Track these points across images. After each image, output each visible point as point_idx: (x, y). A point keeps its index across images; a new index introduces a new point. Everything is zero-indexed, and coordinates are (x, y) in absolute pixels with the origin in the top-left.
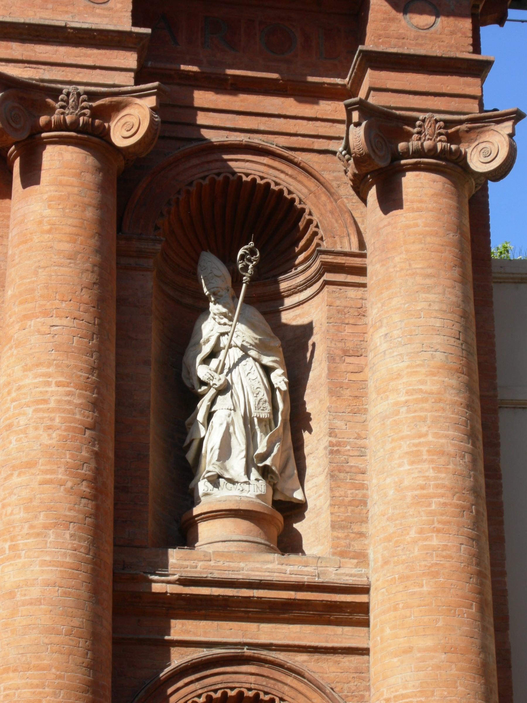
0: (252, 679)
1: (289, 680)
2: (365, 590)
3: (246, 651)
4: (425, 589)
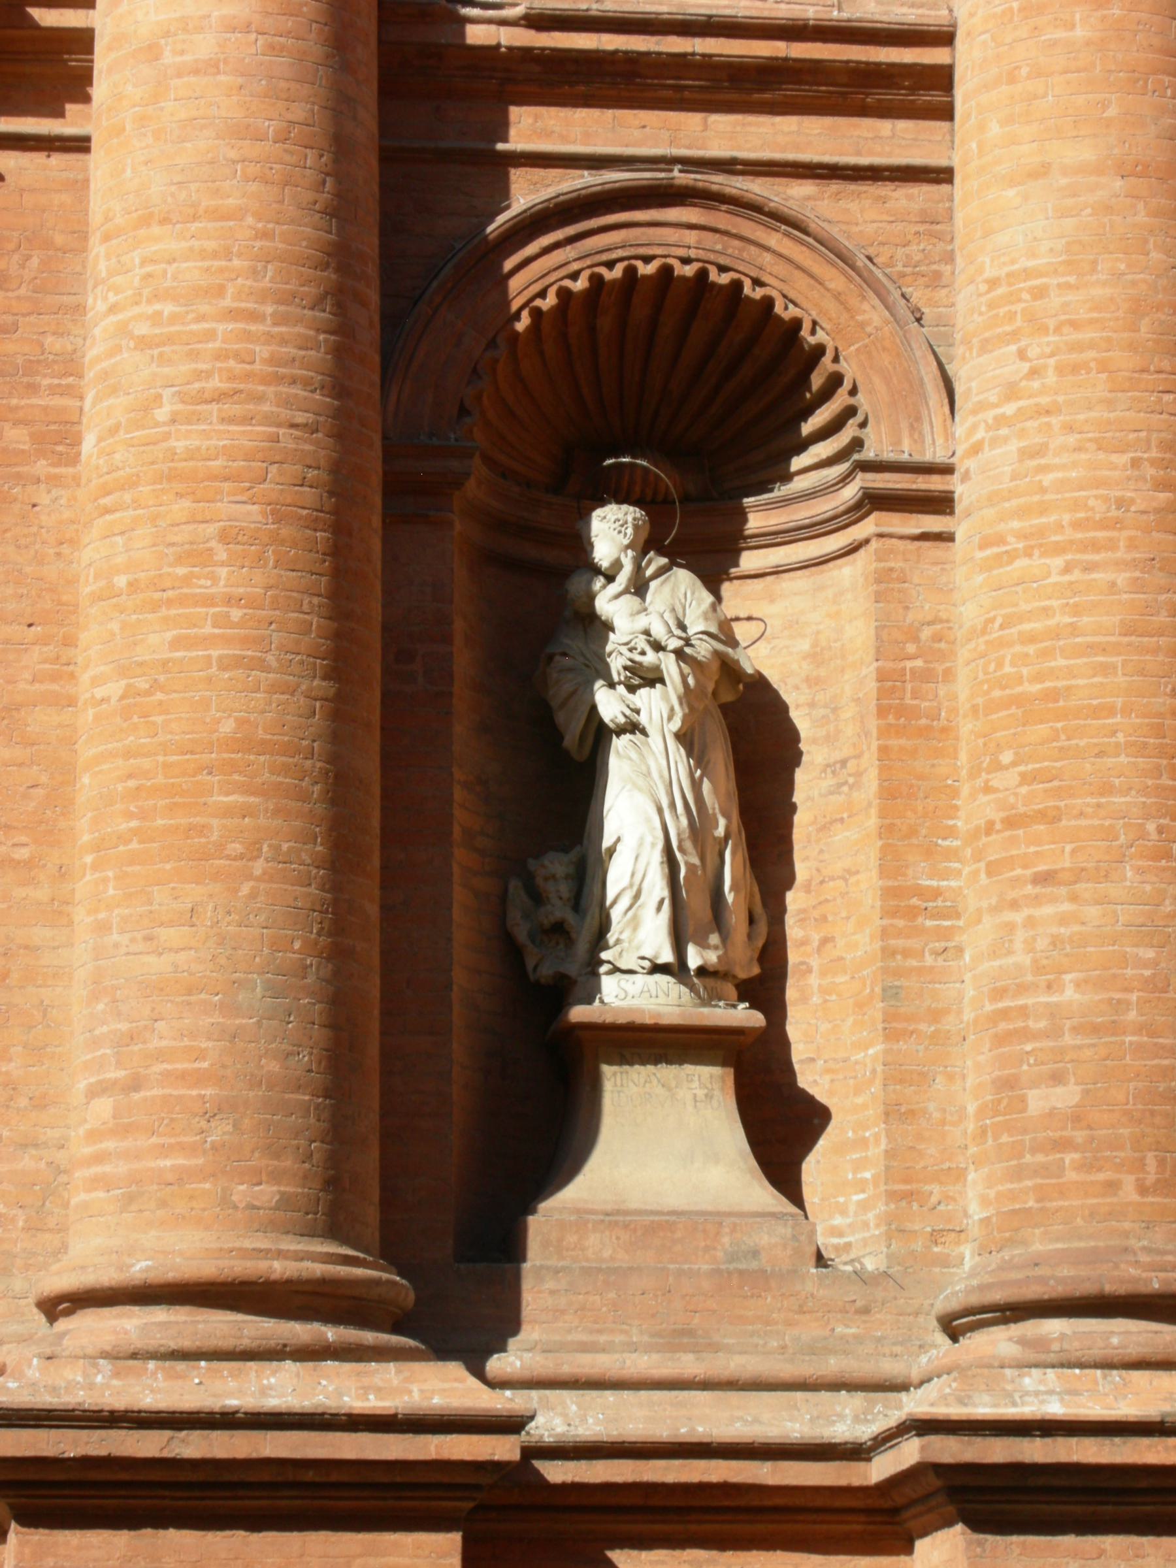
0: (691, 237)
1: (774, 240)
2: (945, 38)
3: (678, 176)
4: (1080, 33)
